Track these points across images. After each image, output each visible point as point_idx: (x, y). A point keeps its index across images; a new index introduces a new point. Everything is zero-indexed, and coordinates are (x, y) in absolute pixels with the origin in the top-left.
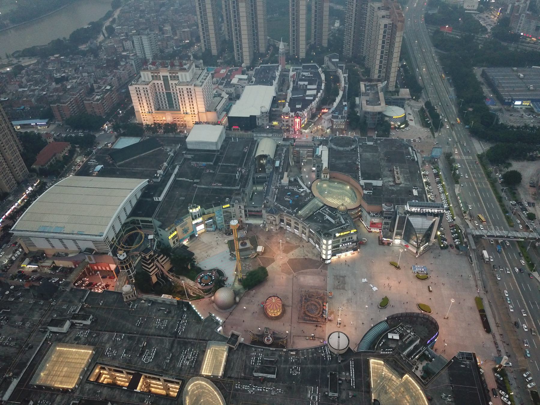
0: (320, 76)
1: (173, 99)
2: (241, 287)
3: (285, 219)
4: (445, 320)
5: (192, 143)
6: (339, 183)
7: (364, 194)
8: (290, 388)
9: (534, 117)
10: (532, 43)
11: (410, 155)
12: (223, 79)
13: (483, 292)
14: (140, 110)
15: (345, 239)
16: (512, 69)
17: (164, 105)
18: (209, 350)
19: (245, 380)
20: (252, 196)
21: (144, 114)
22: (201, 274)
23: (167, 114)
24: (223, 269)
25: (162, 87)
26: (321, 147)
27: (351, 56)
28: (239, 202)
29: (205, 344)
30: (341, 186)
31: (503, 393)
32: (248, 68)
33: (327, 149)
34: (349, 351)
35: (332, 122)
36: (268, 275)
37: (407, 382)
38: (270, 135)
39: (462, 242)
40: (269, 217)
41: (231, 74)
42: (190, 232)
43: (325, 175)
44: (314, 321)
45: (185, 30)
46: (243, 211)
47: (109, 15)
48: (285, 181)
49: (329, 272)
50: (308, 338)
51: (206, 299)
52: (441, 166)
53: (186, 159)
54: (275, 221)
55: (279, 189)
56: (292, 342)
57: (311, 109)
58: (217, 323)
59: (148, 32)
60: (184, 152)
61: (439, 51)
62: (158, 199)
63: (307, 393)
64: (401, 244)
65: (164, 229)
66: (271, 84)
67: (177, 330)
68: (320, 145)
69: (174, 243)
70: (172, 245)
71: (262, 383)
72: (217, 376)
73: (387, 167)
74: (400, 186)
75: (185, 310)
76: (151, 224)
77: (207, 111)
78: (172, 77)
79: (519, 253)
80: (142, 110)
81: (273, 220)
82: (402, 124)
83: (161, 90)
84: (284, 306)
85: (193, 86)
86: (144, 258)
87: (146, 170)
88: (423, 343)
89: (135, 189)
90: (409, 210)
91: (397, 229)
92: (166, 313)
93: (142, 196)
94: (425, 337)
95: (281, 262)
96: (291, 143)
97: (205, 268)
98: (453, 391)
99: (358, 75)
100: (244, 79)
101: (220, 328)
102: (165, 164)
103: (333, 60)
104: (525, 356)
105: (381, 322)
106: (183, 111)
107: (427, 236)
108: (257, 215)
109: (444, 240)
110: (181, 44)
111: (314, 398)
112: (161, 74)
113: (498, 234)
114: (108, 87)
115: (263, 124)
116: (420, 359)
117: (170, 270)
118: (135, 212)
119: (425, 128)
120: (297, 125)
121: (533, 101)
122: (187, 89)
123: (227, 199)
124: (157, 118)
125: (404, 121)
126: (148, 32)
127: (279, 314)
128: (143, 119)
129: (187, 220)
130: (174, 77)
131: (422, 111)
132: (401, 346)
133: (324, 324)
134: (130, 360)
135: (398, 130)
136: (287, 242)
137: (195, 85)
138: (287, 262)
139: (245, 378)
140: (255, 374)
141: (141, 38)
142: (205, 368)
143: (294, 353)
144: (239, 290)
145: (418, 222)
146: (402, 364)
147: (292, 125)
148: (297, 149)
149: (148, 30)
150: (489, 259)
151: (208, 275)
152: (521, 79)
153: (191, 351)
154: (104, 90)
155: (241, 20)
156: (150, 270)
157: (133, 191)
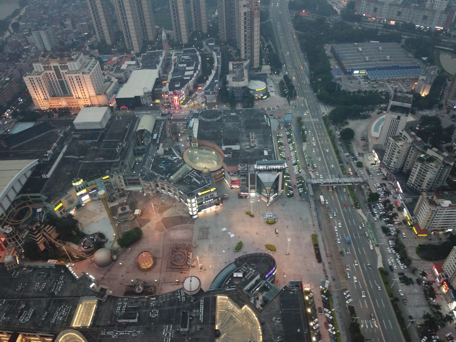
0: (198, 58)
1: (66, 86)
2: (119, 246)
3: (159, 184)
4: (287, 256)
5: (78, 124)
6: (206, 149)
7: (225, 157)
8: (148, 329)
9: (369, 83)
10: (372, 22)
11: (265, 122)
12: (114, 66)
13: (318, 230)
14: (37, 98)
15: (207, 197)
16: (354, 44)
17: (59, 92)
18: (81, 305)
19: (110, 327)
20: (134, 166)
21: (41, 101)
22: (84, 239)
23: (61, 99)
24: (105, 233)
25: (54, 76)
26: (193, 119)
27: (226, 40)
28: (118, 173)
29: (78, 300)
30: (208, 152)
31: (327, 310)
32: (138, 55)
33: (198, 121)
34: (201, 292)
35: (205, 97)
36: (142, 234)
37: (246, 313)
38: (149, 112)
39: (304, 190)
40: (146, 184)
41: (121, 61)
42: (76, 202)
43: (194, 144)
44: (180, 269)
45: (83, 24)
46: (123, 181)
47: (16, 12)
48: (161, 151)
49: (196, 226)
50: (173, 284)
51: (88, 260)
52: (293, 128)
53: (74, 139)
54: (151, 186)
55: (155, 158)
56: (160, 288)
57: (188, 88)
58: (90, 281)
59: (45, 27)
60: (73, 133)
61: (299, 32)
62: (46, 176)
63: (163, 331)
64: (256, 196)
65: (50, 203)
66: (156, 68)
67: (54, 290)
68: (192, 118)
69: (61, 213)
70: (59, 215)
71: (125, 328)
72: (86, 327)
73: (245, 133)
74: (255, 148)
75: (63, 272)
76: (40, 199)
77: (98, 94)
78: (46, 67)
79: (349, 195)
80: (38, 97)
81: (149, 186)
82: (264, 96)
83: (54, 79)
84: (155, 259)
85: (81, 73)
86: (31, 230)
87: (38, 151)
88: (263, 277)
89: (23, 169)
90: (258, 168)
91: (251, 184)
92: (45, 276)
93: (32, 175)
94: (265, 272)
95: (155, 222)
96: (168, 118)
97: (89, 233)
98: (282, 314)
99: (231, 56)
100: (133, 65)
101: (93, 284)
102: (55, 144)
103: (210, 44)
104: (346, 278)
105: (231, 264)
106: (76, 96)
107: (275, 187)
108: (136, 183)
109: (290, 190)
110: (80, 36)
111: (168, 334)
112: (52, 65)
113: (332, 182)
114: (7, 79)
115: (147, 103)
116: (261, 291)
117: (58, 238)
118: (24, 189)
119: (283, 98)
120: (177, 102)
121: (367, 70)
122: (76, 77)
123: (107, 171)
124: (53, 104)
125: (266, 93)
126: (45, 27)
127: (150, 265)
128: (40, 106)
129: (71, 192)
130: (64, 66)
131: (281, 83)
132: (244, 282)
133: (188, 270)
134: (9, 322)
135: (261, 101)
136: (162, 204)
137: (83, 73)
138: (161, 221)
139: (110, 325)
140: (120, 321)
141: (39, 32)
142: (76, 321)
143: (154, 299)
144: (118, 249)
145: (267, 178)
146: (243, 297)
147: (172, 102)
148: (174, 122)
149: (46, 25)
150: (325, 202)
151: (91, 239)
152: (361, 52)
153: (64, 307)
154: (4, 82)
155: (127, 13)
156: (37, 240)
157: (22, 171)
